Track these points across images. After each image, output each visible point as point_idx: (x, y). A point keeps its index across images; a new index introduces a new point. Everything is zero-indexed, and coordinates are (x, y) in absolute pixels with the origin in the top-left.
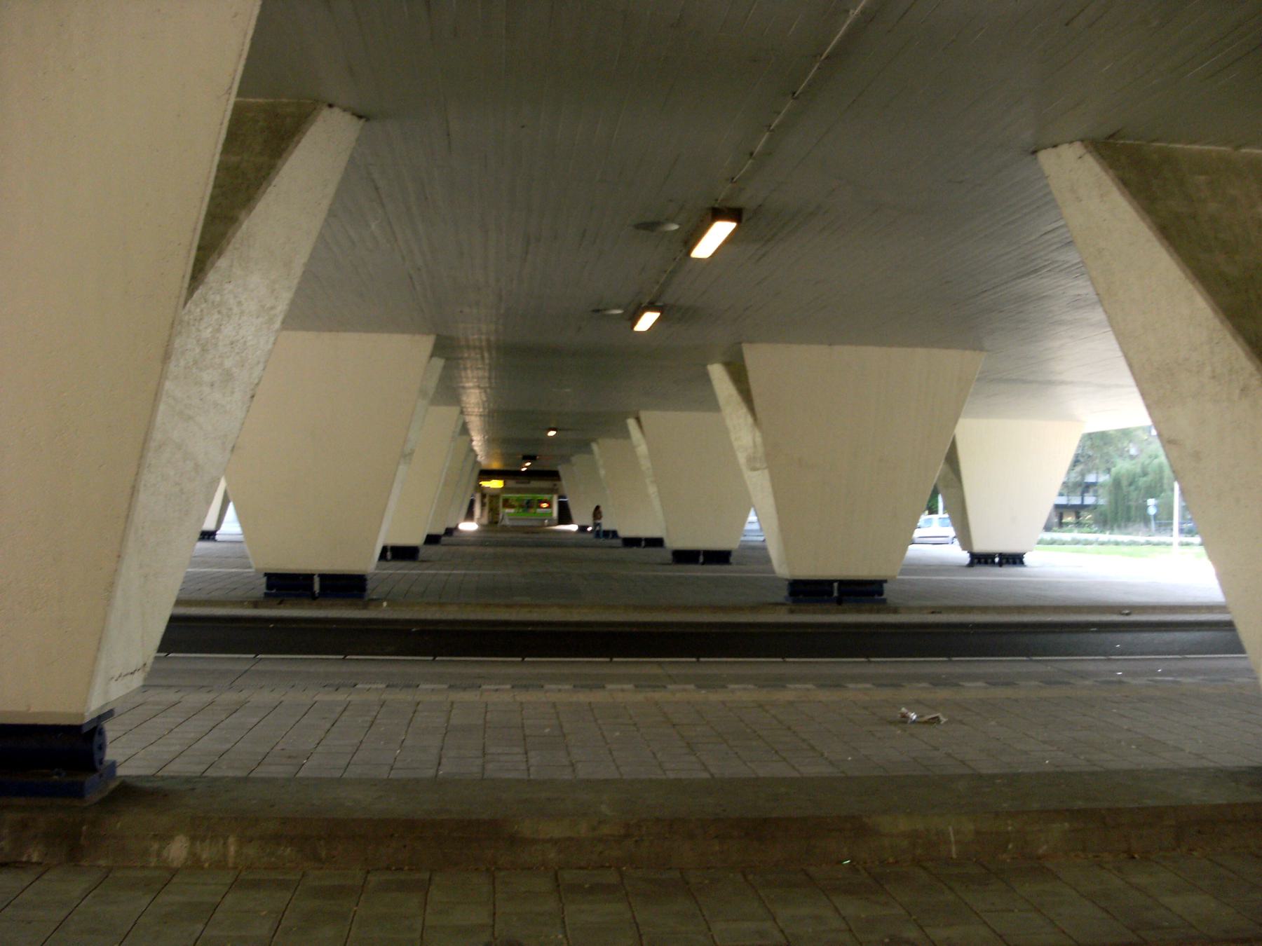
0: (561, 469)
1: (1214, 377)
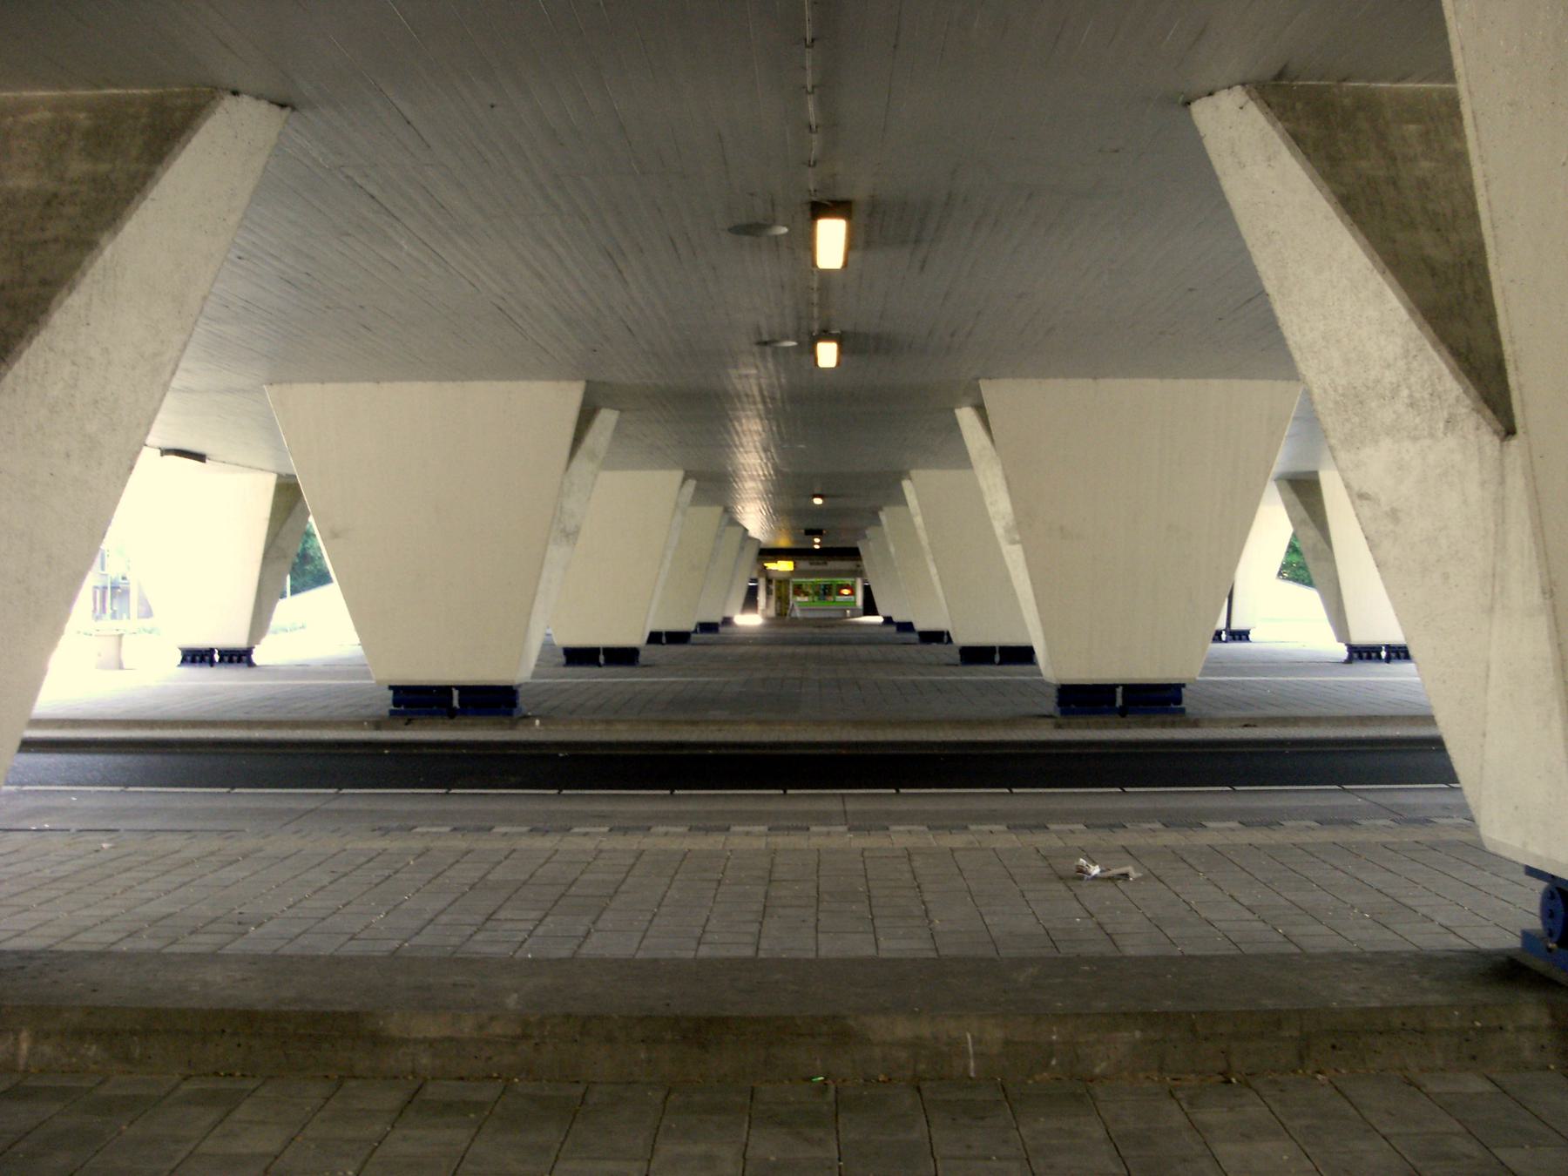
0: (860, 545)
1: (1412, 405)
